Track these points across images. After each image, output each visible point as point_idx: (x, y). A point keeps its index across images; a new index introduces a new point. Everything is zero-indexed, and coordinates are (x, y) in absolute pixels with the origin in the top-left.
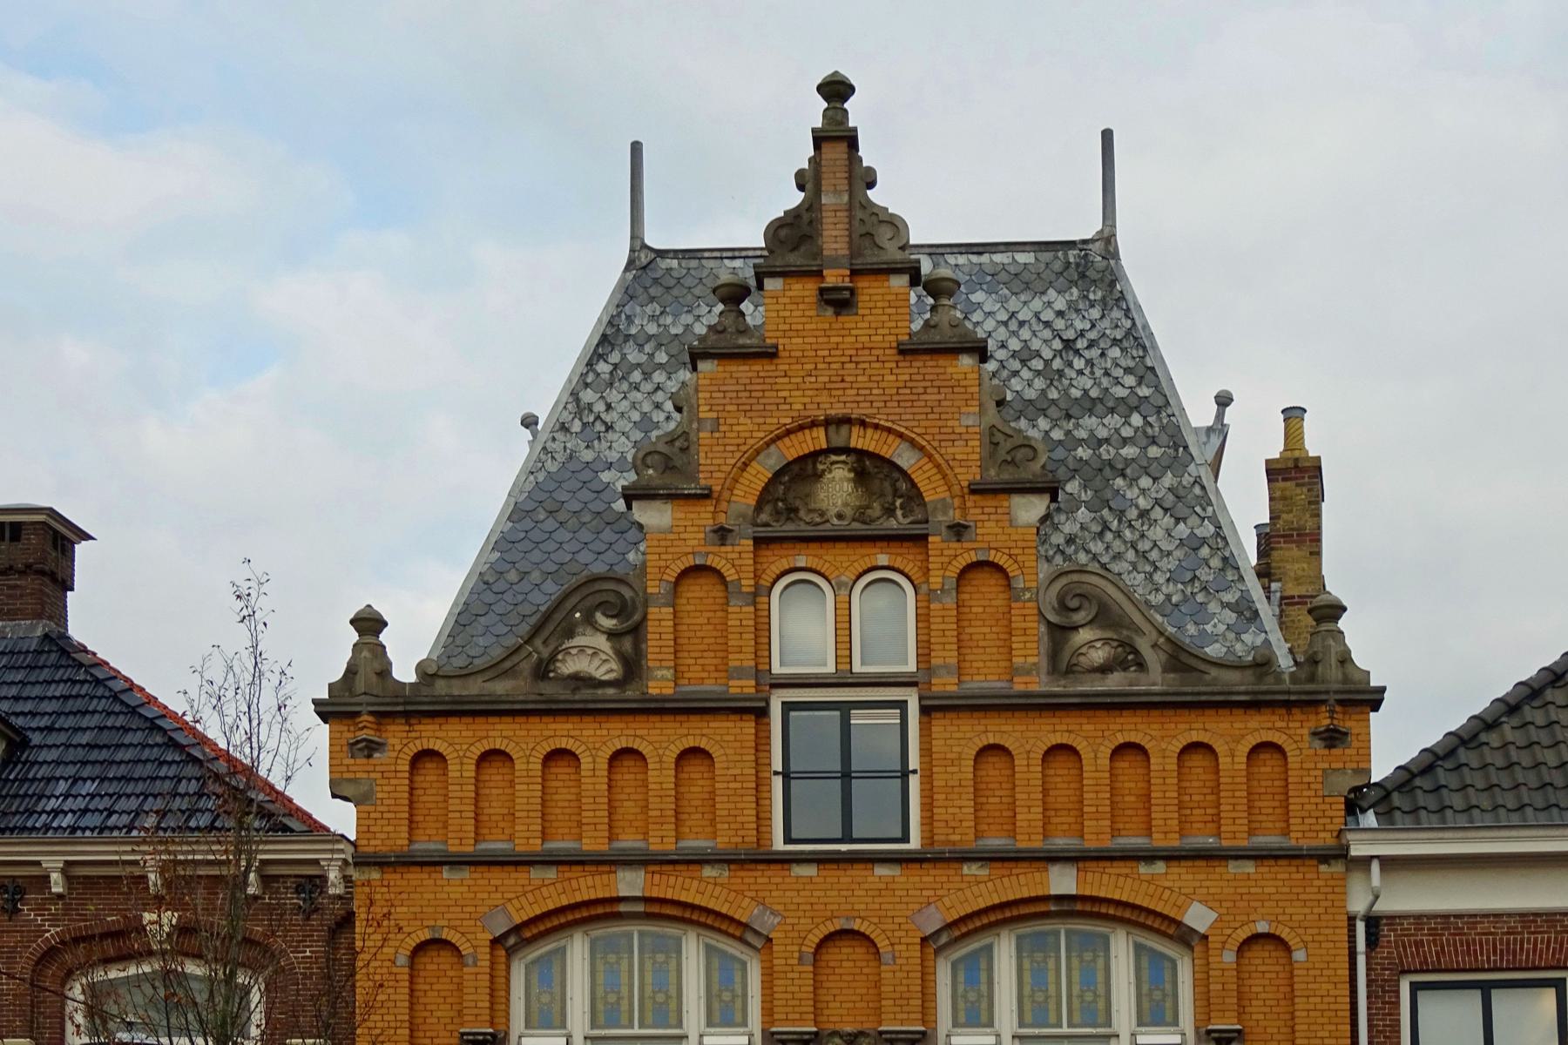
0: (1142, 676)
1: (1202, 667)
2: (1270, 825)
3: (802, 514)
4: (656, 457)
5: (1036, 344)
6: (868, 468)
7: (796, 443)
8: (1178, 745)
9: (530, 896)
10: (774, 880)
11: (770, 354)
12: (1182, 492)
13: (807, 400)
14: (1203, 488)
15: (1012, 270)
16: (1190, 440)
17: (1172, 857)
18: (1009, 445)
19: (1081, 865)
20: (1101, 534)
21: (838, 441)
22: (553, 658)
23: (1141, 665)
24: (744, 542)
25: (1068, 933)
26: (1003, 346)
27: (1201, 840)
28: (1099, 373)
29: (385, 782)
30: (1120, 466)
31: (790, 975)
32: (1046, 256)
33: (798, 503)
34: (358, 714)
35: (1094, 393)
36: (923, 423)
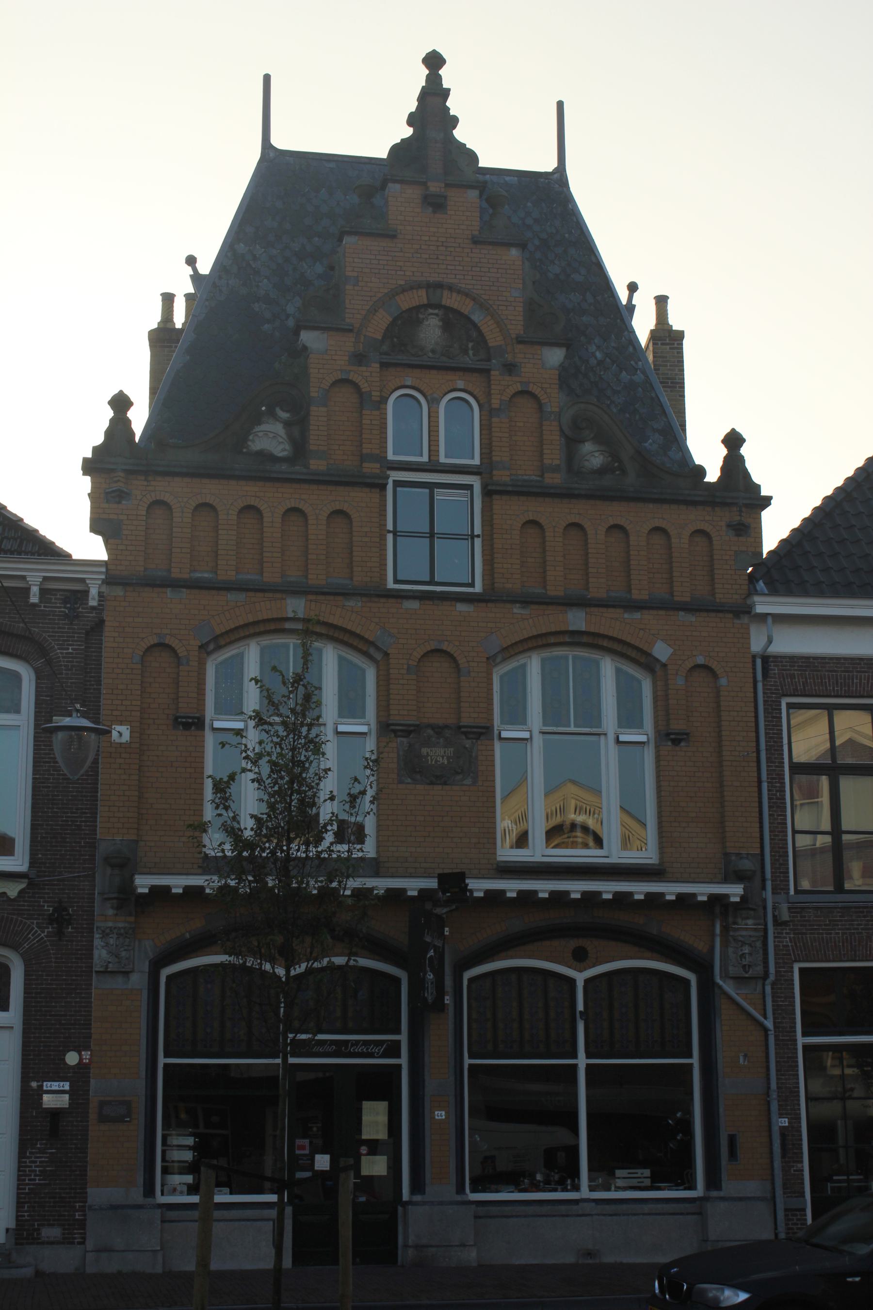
6: (453, 321)
24: (374, 365)
25: (574, 657)
31: (401, 682)
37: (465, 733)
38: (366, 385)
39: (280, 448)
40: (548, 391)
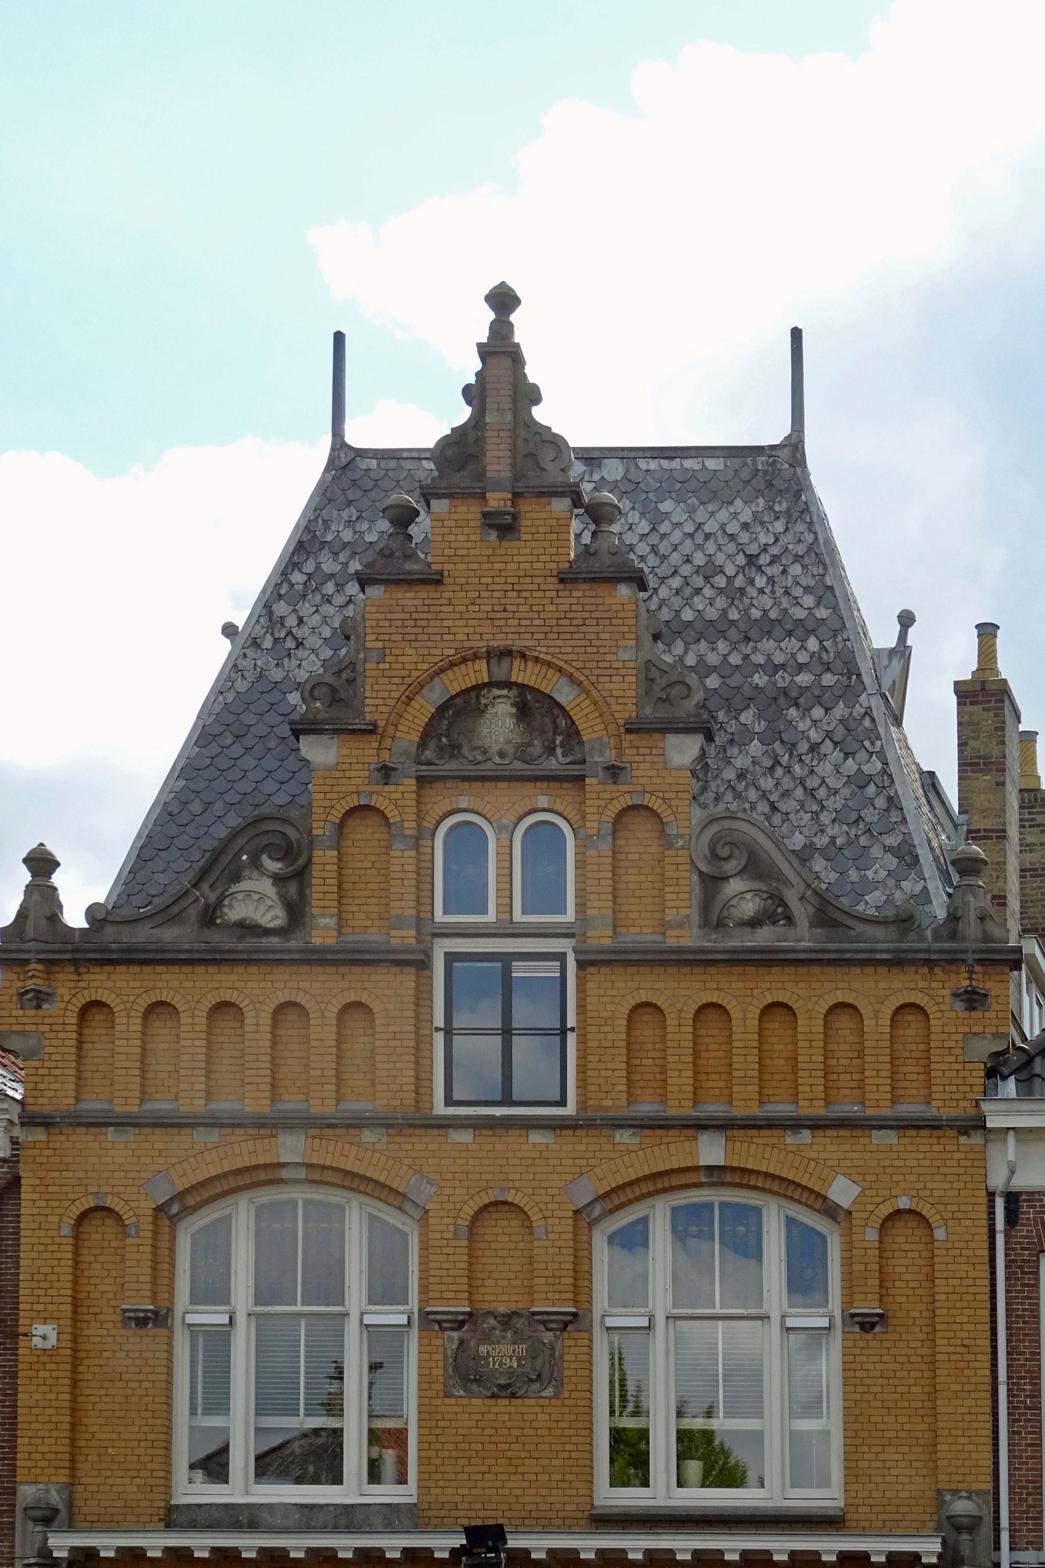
0: (790, 932)
1: (849, 922)
2: (914, 1092)
3: (465, 751)
4: (324, 689)
5: (720, 559)
6: (531, 705)
7: (459, 675)
8: (824, 1006)
9: (192, 1160)
10: (432, 1147)
11: (436, 581)
12: (852, 725)
13: (470, 630)
14: (873, 720)
15: (701, 477)
16: (865, 667)
17: (817, 1125)
18: (664, 681)
19: (729, 1133)
20: (772, 769)
21: (499, 675)
22: (219, 903)
23: (790, 920)
24: (407, 781)
26: (688, 561)
27: (847, 1108)
28: (779, 591)
29: (53, 1035)
30: (794, 695)
31: (445, 1250)
32: (734, 463)
33: (461, 740)
34: (27, 961)
35: (773, 614)
36: (582, 657)
37: (544, 1323)
38: (396, 812)
39: (272, 916)
40: (674, 803)
